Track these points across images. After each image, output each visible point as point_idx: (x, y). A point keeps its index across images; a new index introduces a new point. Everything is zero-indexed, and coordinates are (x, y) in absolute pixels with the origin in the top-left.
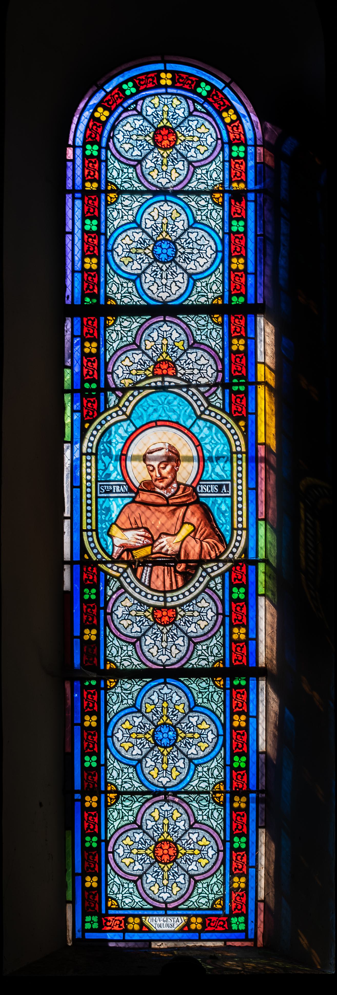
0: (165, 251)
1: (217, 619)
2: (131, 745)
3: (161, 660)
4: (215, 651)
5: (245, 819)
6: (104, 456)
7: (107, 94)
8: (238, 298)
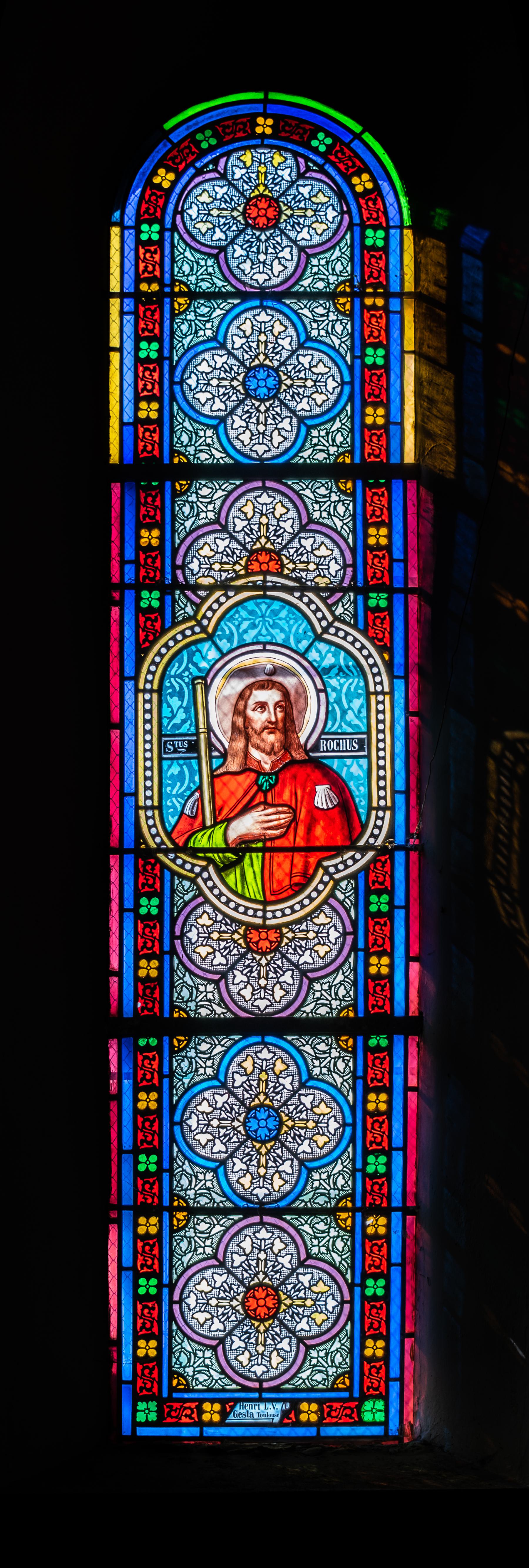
0: (262, 1302)
1: (345, 573)
2: (210, 950)
3: (256, 451)
4: (338, 1359)
5: (387, 929)
6: (171, 697)
7: (175, 146)
8: (375, 362)
